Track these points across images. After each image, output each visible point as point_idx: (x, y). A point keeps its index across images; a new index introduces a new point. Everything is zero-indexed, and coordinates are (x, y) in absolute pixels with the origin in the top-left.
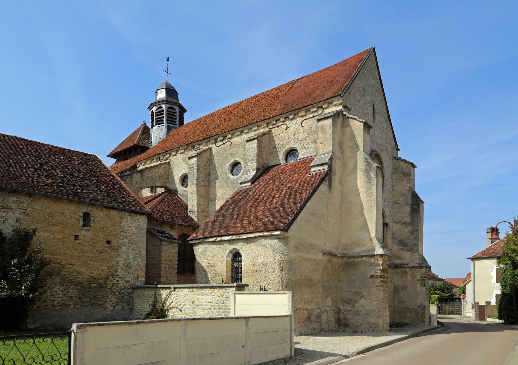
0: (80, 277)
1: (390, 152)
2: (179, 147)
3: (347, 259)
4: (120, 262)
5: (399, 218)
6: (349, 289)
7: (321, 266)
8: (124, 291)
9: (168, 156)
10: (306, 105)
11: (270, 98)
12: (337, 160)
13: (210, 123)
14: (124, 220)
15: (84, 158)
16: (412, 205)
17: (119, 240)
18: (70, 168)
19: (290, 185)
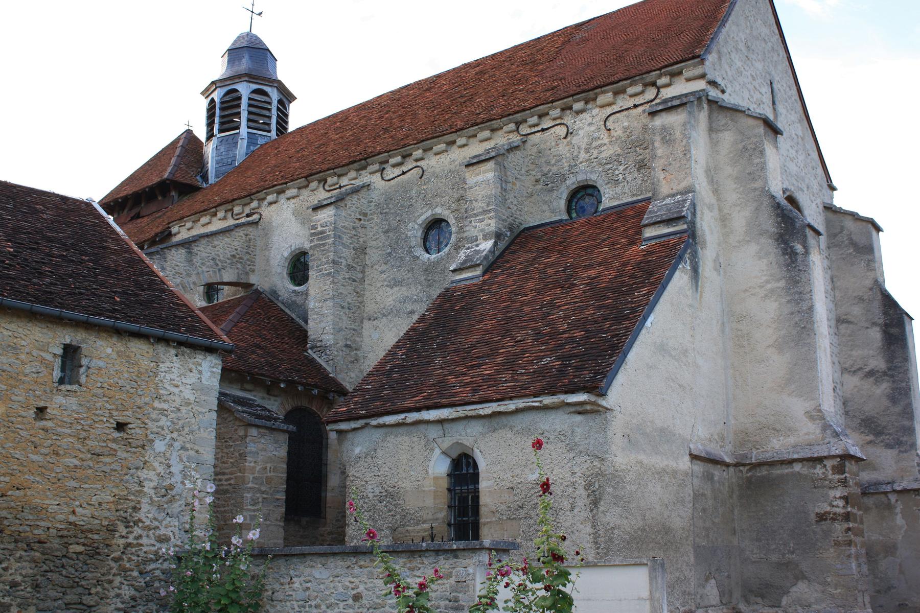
0: (42, 524)
1: (816, 195)
2: (286, 183)
3: (749, 470)
4: (146, 483)
5: (855, 361)
6: (762, 556)
7: (689, 491)
8: (153, 566)
9: (255, 204)
10: (612, 79)
11: (514, 67)
12: (706, 211)
13: (363, 126)
14: (163, 367)
15: (62, 209)
16: (886, 325)
17: (147, 421)
18: (30, 233)
19: (592, 273)
